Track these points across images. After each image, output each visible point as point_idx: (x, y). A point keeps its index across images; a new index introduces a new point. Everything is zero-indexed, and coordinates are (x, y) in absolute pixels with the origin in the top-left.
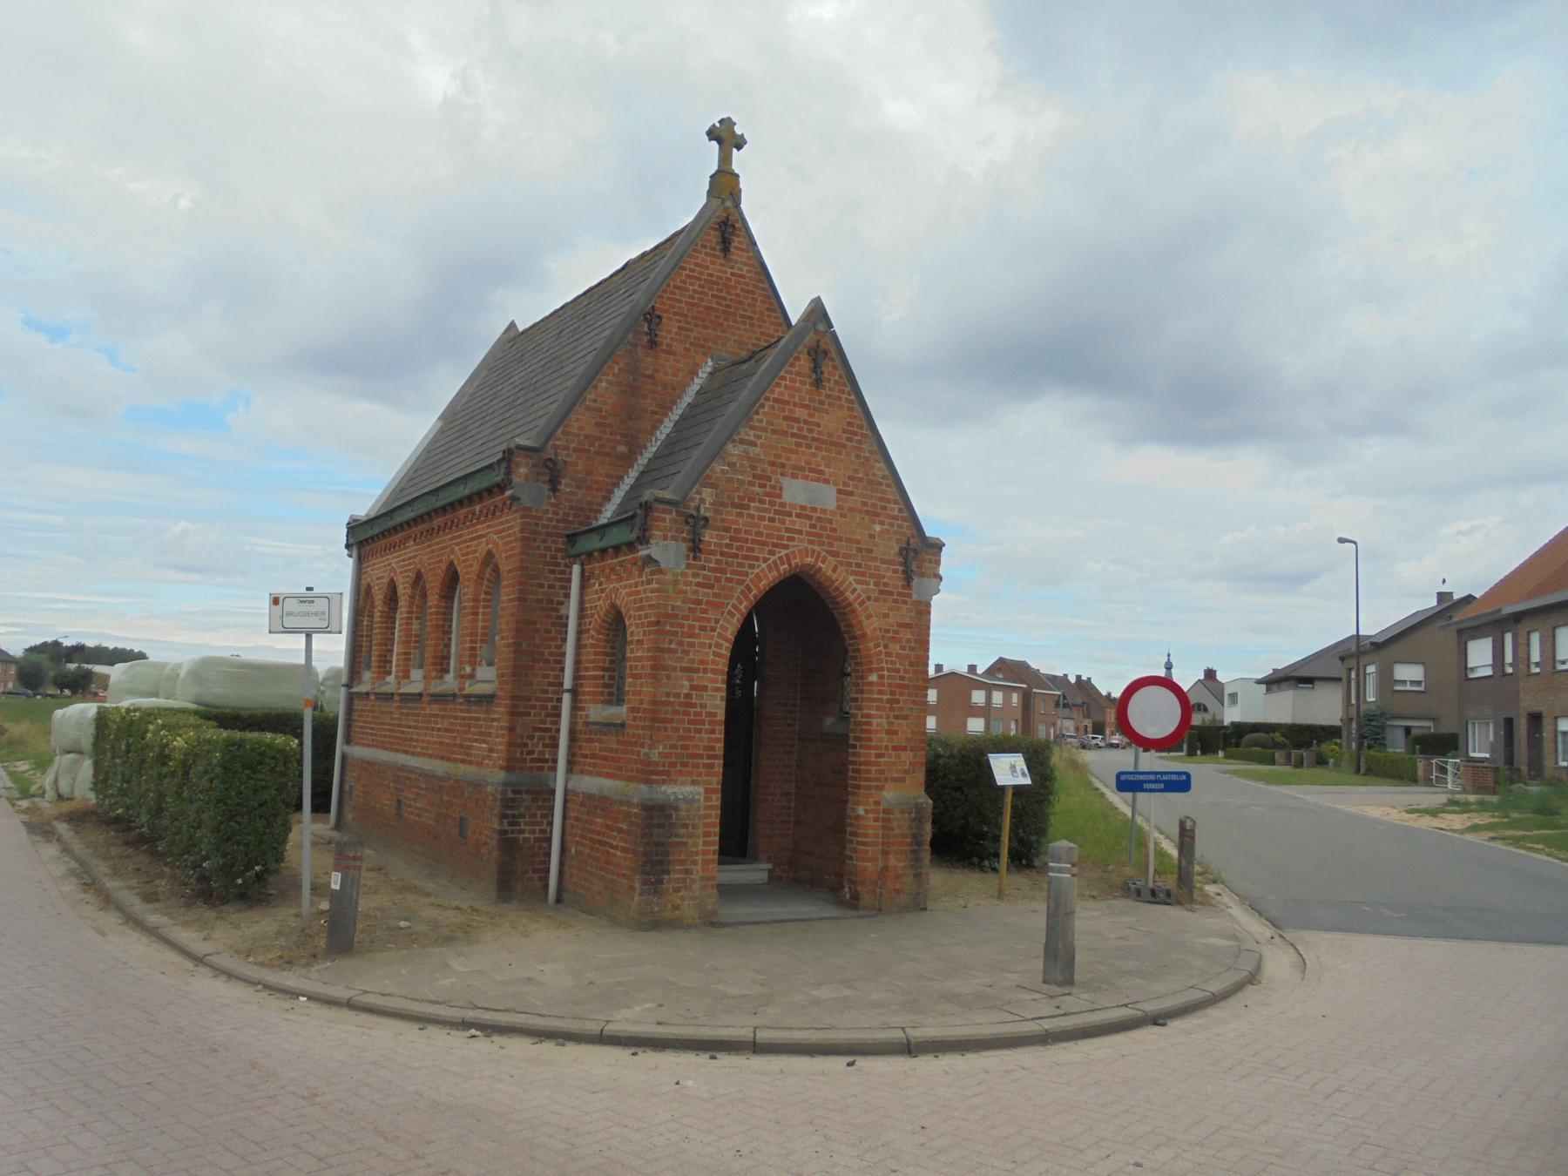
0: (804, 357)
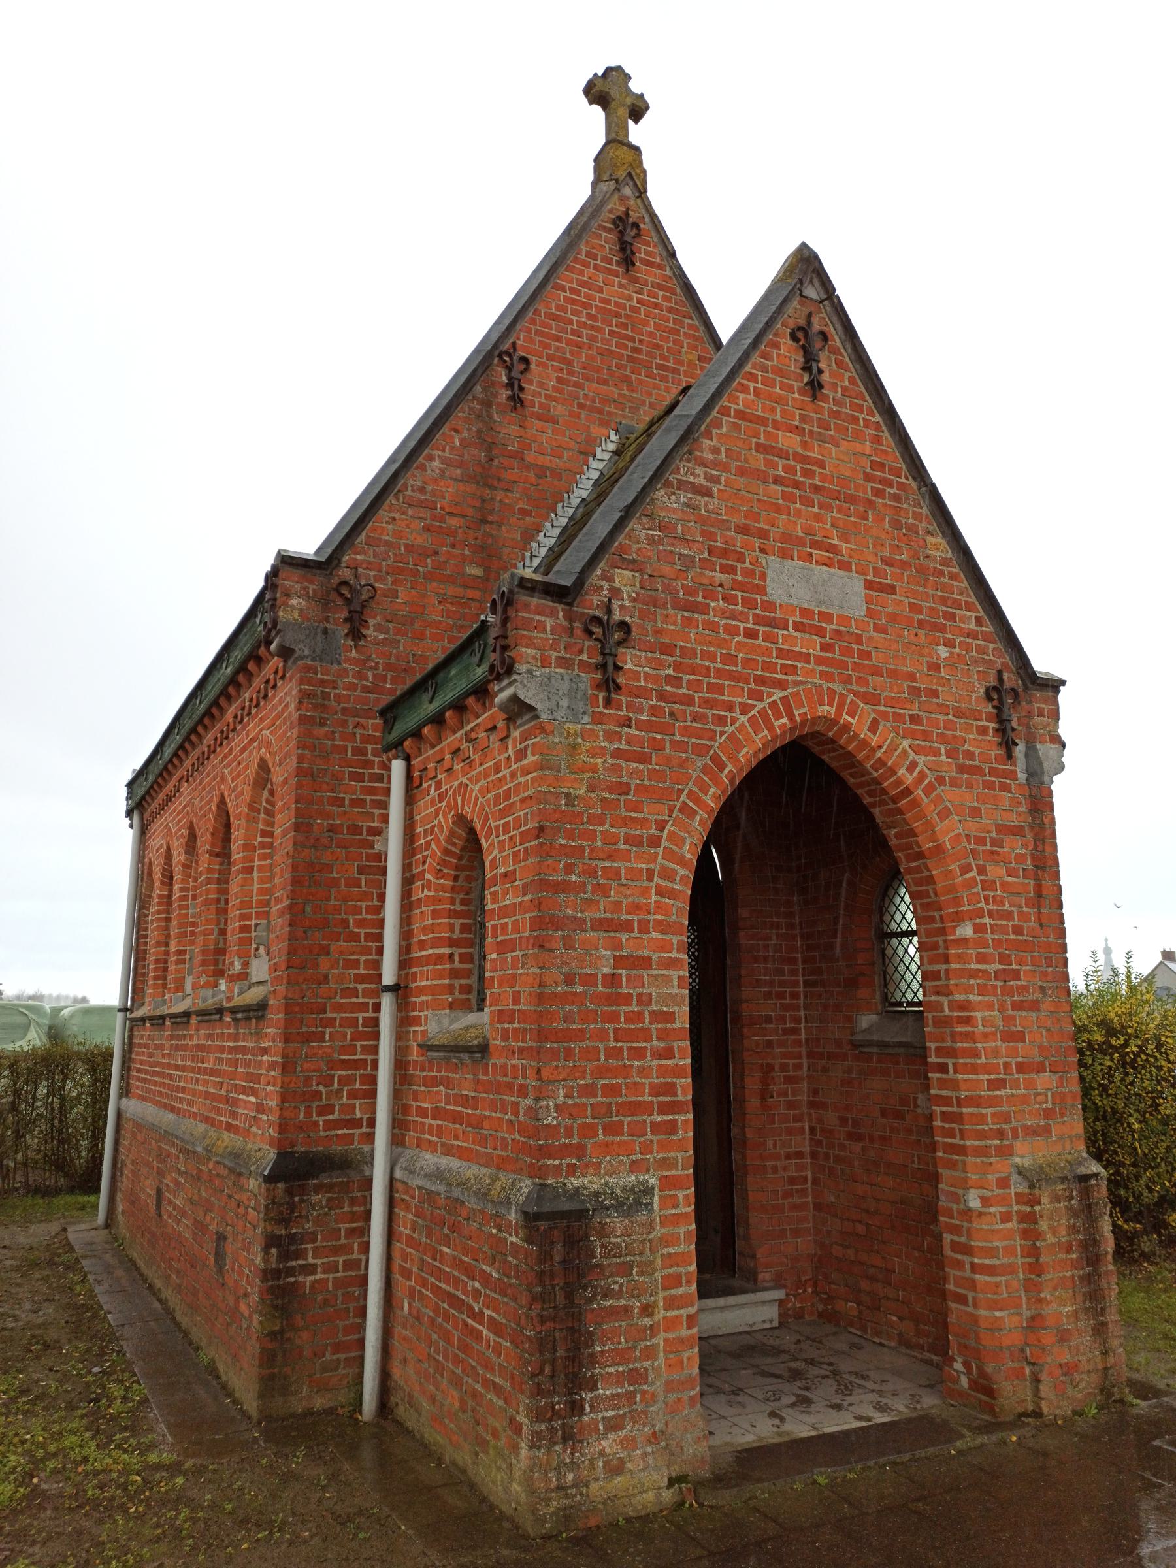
0: (786, 343)
